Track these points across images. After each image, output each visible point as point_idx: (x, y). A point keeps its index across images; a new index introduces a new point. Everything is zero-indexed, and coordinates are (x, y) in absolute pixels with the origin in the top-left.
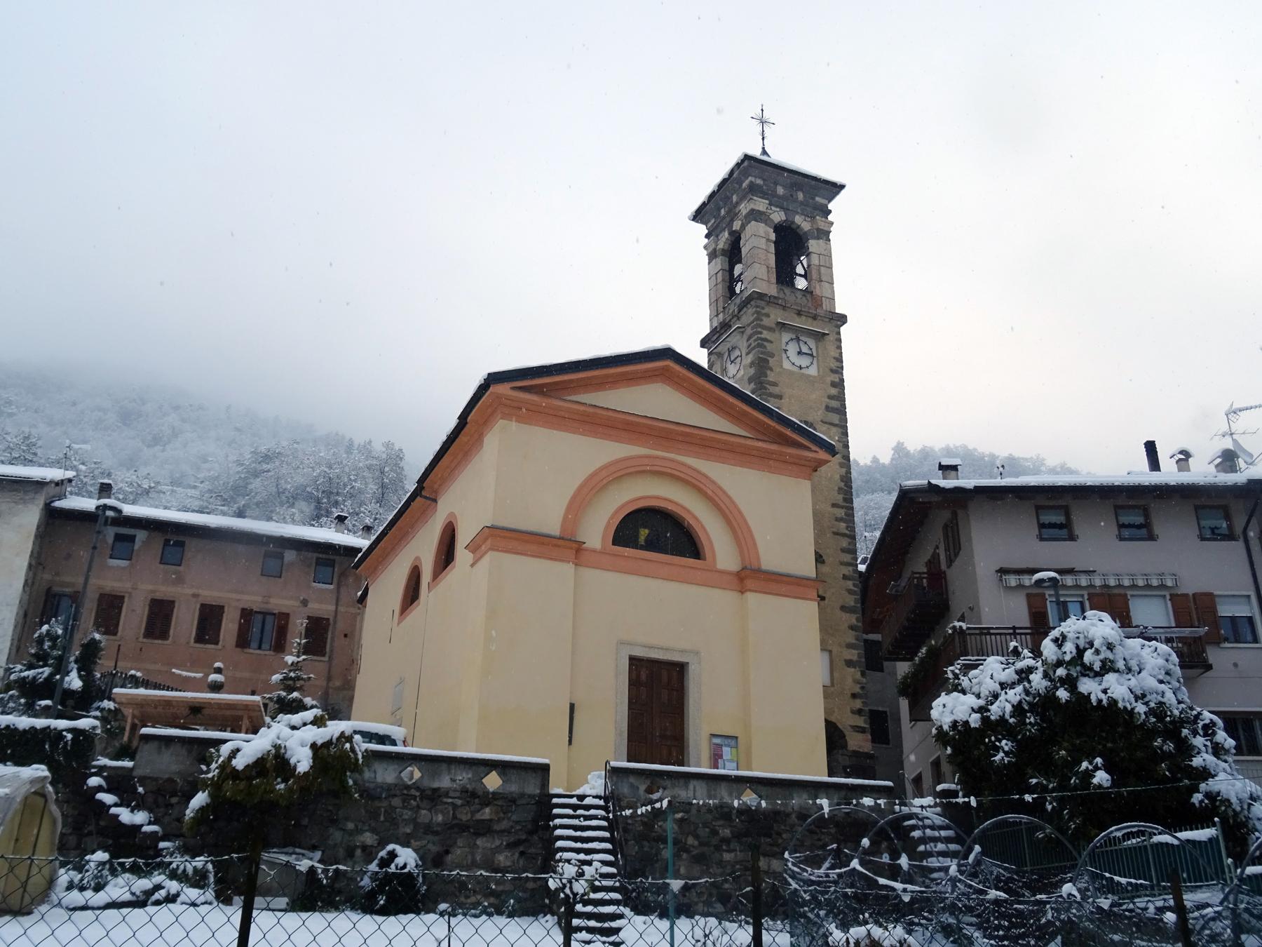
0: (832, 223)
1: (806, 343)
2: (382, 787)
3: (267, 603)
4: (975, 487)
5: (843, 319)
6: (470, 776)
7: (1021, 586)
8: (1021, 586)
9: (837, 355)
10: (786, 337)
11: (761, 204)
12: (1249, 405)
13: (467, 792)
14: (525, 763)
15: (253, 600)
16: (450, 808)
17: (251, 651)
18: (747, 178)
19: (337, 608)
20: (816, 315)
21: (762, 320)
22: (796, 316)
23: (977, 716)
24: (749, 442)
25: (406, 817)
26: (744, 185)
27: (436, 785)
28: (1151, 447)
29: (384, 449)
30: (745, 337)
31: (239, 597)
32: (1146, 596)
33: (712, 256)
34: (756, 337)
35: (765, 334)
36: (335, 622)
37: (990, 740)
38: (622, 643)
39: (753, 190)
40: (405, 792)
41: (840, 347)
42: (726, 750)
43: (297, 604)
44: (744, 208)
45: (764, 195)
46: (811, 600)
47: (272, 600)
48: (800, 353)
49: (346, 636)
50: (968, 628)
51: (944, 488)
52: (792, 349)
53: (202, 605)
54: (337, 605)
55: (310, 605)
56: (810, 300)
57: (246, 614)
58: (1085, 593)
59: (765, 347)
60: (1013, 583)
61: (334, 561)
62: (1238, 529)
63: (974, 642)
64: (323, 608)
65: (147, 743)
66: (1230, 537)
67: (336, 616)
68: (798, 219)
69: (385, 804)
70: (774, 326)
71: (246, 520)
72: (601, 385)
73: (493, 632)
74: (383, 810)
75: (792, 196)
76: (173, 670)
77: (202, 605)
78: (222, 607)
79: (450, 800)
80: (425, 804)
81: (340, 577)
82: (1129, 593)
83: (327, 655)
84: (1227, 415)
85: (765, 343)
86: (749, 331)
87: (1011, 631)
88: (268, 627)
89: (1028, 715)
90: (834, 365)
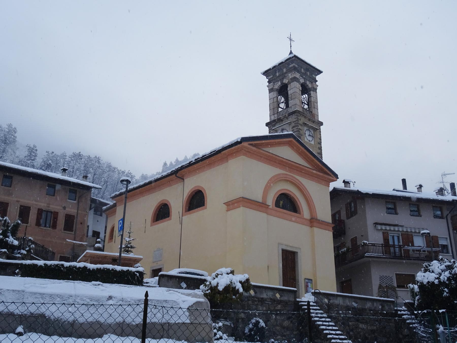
0: (318, 86)
1: (311, 131)
2: (245, 297)
3: (49, 207)
4: (373, 194)
5: (321, 124)
6: (272, 294)
7: (381, 229)
8: (381, 229)
9: (320, 137)
10: (305, 128)
11: (297, 75)
12: (449, 173)
13: (272, 299)
14: (273, 288)
15: (43, 205)
16: (268, 305)
17: (42, 228)
18: (293, 64)
19: (78, 211)
20: (314, 121)
21: (299, 121)
22: (308, 121)
23: (437, 280)
24: (312, 171)
25: (254, 308)
26: (290, 66)
27: (262, 297)
28: (404, 181)
29: (7, 127)
30: (291, 127)
31: (37, 203)
32: (417, 236)
33: (271, 91)
34: (297, 127)
35: (300, 127)
36: (77, 218)
37: (441, 288)
38: (279, 244)
39: (295, 69)
40: (253, 299)
41: (320, 134)
42: (309, 284)
43: (61, 208)
44: (290, 76)
45: (298, 72)
46: (330, 231)
47: (51, 206)
48: (310, 135)
49: (81, 223)
50: (369, 243)
51: (363, 193)
52: (307, 133)
53: (21, 206)
54: (78, 210)
55: (67, 209)
56: (311, 115)
57: (40, 212)
58: (400, 233)
59: (300, 132)
60: (379, 228)
61: (76, 190)
62: (445, 215)
63: (376, 248)
64: (72, 211)
65: (163, 278)
66: (442, 217)
67: (77, 215)
68: (308, 83)
69: (246, 303)
70: (302, 124)
71: (34, 169)
72: (272, 145)
73: (245, 238)
74: (246, 305)
75: (306, 73)
76: (67, 240)
77: (21, 206)
78: (30, 207)
79: (267, 302)
80: (260, 303)
81: (79, 198)
82: (389, 232)
83: (74, 231)
84: (442, 176)
85: (300, 130)
86: (293, 124)
87: (381, 245)
88: (49, 218)
89: (452, 281)
90: (319, 141)
